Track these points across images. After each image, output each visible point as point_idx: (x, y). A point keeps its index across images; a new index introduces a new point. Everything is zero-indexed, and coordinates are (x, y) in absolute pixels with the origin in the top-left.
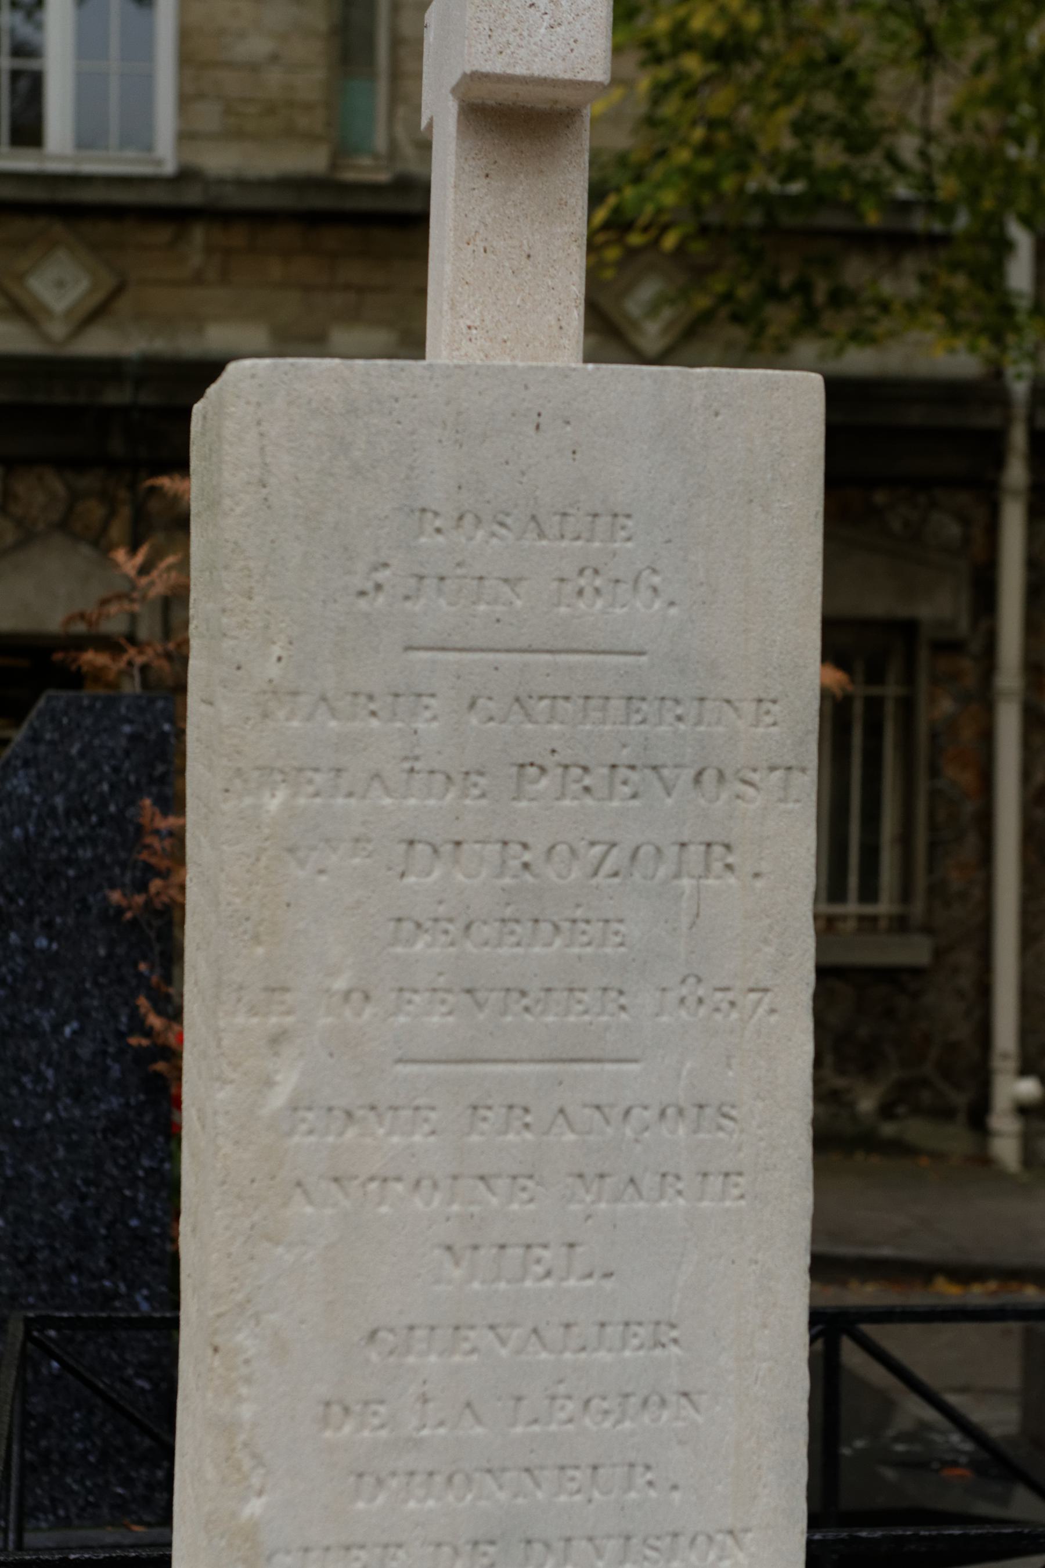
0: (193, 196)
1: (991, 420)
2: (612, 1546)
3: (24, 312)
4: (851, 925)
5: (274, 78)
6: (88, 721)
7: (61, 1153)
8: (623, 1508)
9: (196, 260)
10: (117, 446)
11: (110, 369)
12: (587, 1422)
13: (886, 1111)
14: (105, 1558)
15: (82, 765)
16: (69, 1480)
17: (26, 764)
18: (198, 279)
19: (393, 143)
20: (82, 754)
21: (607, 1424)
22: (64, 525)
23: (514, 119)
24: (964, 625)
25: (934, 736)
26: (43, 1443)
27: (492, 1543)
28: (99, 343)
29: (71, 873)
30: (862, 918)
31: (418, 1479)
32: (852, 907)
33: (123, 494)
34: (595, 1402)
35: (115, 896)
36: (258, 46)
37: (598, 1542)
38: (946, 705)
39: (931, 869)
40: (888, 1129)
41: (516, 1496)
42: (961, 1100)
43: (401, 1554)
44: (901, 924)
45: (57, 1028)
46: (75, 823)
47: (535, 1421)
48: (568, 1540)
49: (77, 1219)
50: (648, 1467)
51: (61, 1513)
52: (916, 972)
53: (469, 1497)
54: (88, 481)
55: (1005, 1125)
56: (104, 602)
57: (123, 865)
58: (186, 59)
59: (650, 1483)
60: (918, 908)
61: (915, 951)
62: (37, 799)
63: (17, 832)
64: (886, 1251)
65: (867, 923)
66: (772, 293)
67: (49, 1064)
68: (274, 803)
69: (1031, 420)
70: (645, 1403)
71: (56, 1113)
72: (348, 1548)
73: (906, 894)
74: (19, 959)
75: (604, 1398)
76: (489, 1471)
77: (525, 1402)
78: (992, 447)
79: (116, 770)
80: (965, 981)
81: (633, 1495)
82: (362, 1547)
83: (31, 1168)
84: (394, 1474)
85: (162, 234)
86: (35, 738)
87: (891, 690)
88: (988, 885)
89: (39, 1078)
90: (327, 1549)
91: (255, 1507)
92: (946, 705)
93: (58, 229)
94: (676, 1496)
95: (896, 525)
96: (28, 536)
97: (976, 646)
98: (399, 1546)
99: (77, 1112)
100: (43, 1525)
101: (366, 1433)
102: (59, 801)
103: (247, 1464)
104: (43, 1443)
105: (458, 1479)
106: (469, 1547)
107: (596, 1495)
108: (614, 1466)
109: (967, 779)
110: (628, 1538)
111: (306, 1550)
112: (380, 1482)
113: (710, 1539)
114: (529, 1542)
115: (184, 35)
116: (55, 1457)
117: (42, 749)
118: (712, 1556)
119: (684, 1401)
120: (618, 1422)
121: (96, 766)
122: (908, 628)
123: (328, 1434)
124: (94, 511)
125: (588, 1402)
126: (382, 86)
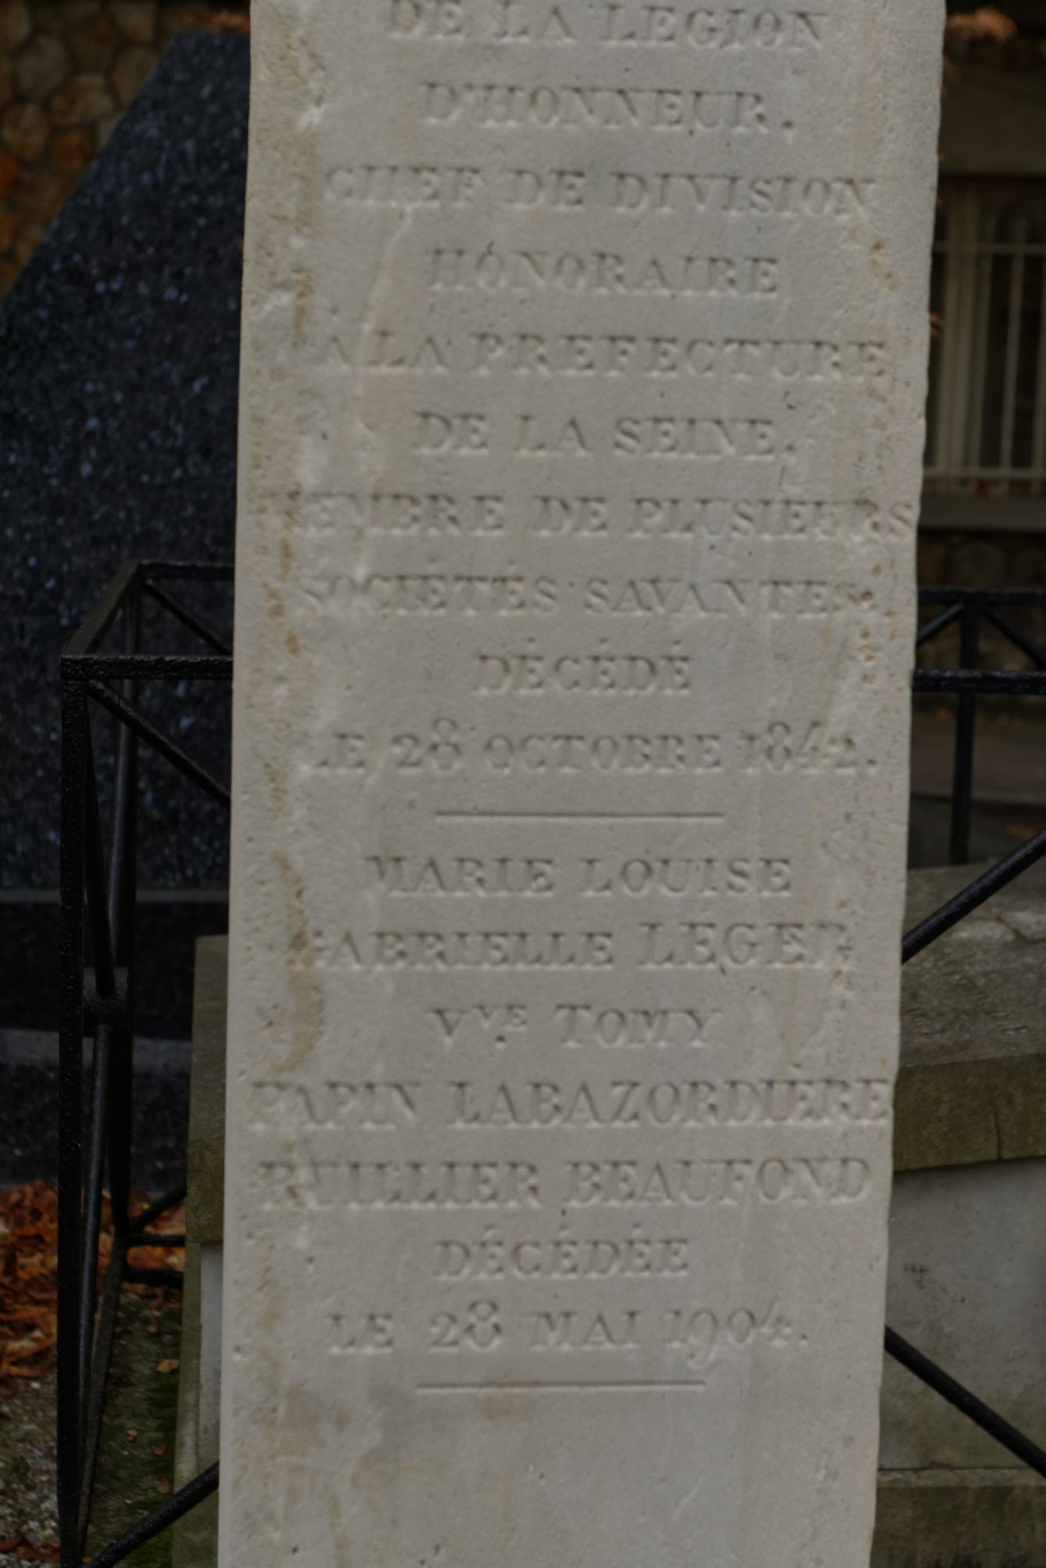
2: (716, 187)
4: (1003, 489)
6: (220, 62)
7: (190, 510)
8: (728, 144)
12: (691, 40)
14: (202, 661)
15: (213, 109)
16: (196, 840)
17: (156, 106)
20: (213, 97)
21: (713, 45)
26: (172, 803)
27: (580, 174)
29: (202, 222)
30: (1014, 484)
31: (498, 94)
32: (1005, 471)
34: (701, 17)
37: (699, 181)
41: (607, 121)
43: (477, 180)
45: (187, 382)
46: (205, 170)
47: (631, 36)
48: (666, 176)
50: (758, 99)
51: (189, 872)
53: (555, 119)
59: (760, 118)
62: (167, 143)
63: (146, 178)
64: (1027, 798)
65: (1020, 487)
67: (178, 419)
70: (757, 22)
71: (185, 470)
72: (417, 170)
74: (148, 310)
75: (710, 14)
76: (577, 90)
77: (621, 12)
81: (741, 130)
82: (433, 170)
83: (159, 525)
84: (470, 87)
89: (168, 432)
90: (394, 169)
91: (312, 116)
94: (790, 135)
98: (475, 171)
99: (207, 470)
100: (172, 884)
101: (439, 37)
102: (189, 146)
103: (305, 64)
104: (172, 803)
105: (543, 97)
106: (553, 177)
107: (699, 127)
108: (720, 93)
110: (733, 180)
111: (370, 168)
112: (454, 96)
113: (827, 187)
114: (621, 176)
116: (183, 816)
118: (828, 208)
119: (801, 23)
120: (725, 43)
123: (396, 35)
125: (692, 16)
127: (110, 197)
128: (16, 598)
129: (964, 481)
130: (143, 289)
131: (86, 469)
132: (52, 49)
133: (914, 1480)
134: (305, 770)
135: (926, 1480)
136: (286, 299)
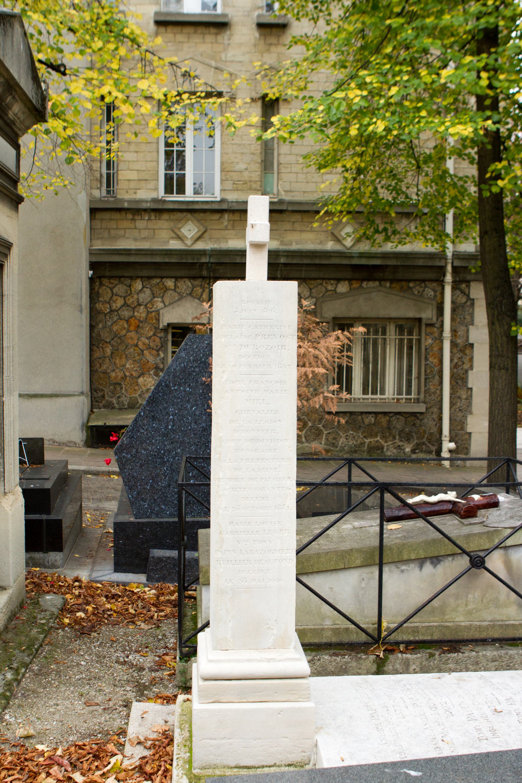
0: (224, 206)
1: (442, 263)
3: (179, 238)
5: (246, 174)
9: (226, 223)
10: (205, 273)
11: (203, 253)
13: (413, 451)
17: (184, 350)
18: (226, 229)
19: (278, 190)
20: (196, 348)
22: (190, 294)
23: (258, 246)
24: (435, 319)
25: (426, 349)
28: (200, 246)
30: (406, 399)
33: (206, 286)
35: (204, 379)
36: (242, 166)
38: (430, 341)
39: (425, 386)
40: (414, 456)
42: (434, 448)
44: (417, 401)
45: (191, 408)
49: (196, 450)
52: (421, 413)
54: (198, 282)
55: (445, 454)
56: (201, 314)
57: (206, 372)
58: (222, 170)
60: (422, 396)
61: (421, 408)
66: (377, 231)
68: (223, 340)
69: (452, 263)
73: (419, 393)
78: (442, 270)
79: (204, 351)
80: (435, 416)
85: (217, 216)
86: (186, 345)
87: (415, 337)
88: (441, 390)
89: (187, 419)
91: (221, 434)
92: (430, 341)
93: (189, 215)
95: (416, 292)
96: (181, 297)
97: (437, 325)
102: (191, 358)
109: (436, 361)
115: (222, 164)
117: (188, 347)
121: (199, 350)
122: (420, 320)
124: (199, 290)
126: (276, 175)
127: (174, 369)
128: (155, 455)
129: (393, 399)
130: (182, 388)
131: (170, 427)
132: (148, 292)
133: (331, 627)
134: (221, 512)
135: (334, 627)
136: (218, 456)
